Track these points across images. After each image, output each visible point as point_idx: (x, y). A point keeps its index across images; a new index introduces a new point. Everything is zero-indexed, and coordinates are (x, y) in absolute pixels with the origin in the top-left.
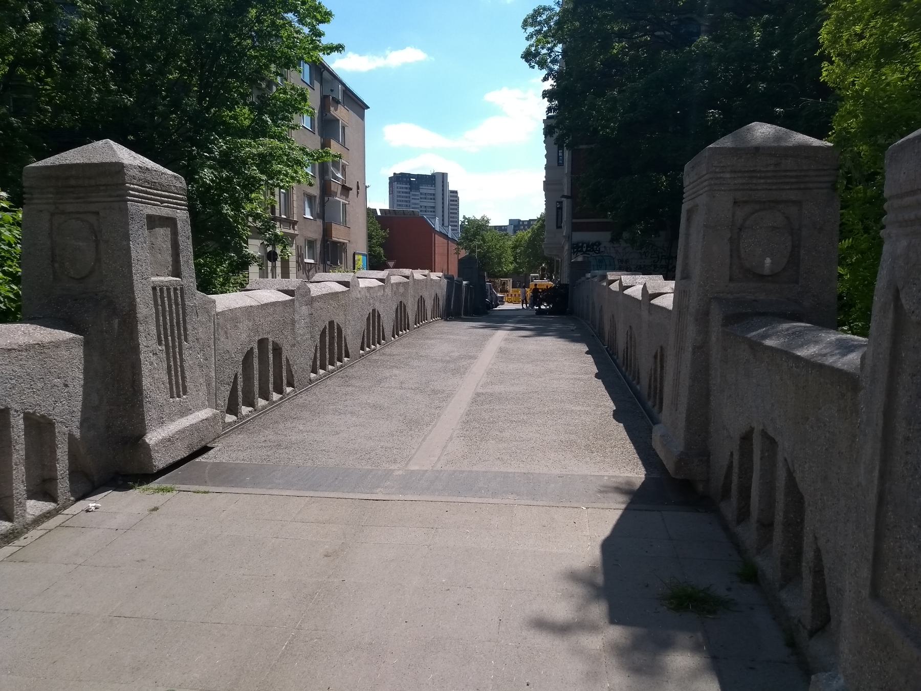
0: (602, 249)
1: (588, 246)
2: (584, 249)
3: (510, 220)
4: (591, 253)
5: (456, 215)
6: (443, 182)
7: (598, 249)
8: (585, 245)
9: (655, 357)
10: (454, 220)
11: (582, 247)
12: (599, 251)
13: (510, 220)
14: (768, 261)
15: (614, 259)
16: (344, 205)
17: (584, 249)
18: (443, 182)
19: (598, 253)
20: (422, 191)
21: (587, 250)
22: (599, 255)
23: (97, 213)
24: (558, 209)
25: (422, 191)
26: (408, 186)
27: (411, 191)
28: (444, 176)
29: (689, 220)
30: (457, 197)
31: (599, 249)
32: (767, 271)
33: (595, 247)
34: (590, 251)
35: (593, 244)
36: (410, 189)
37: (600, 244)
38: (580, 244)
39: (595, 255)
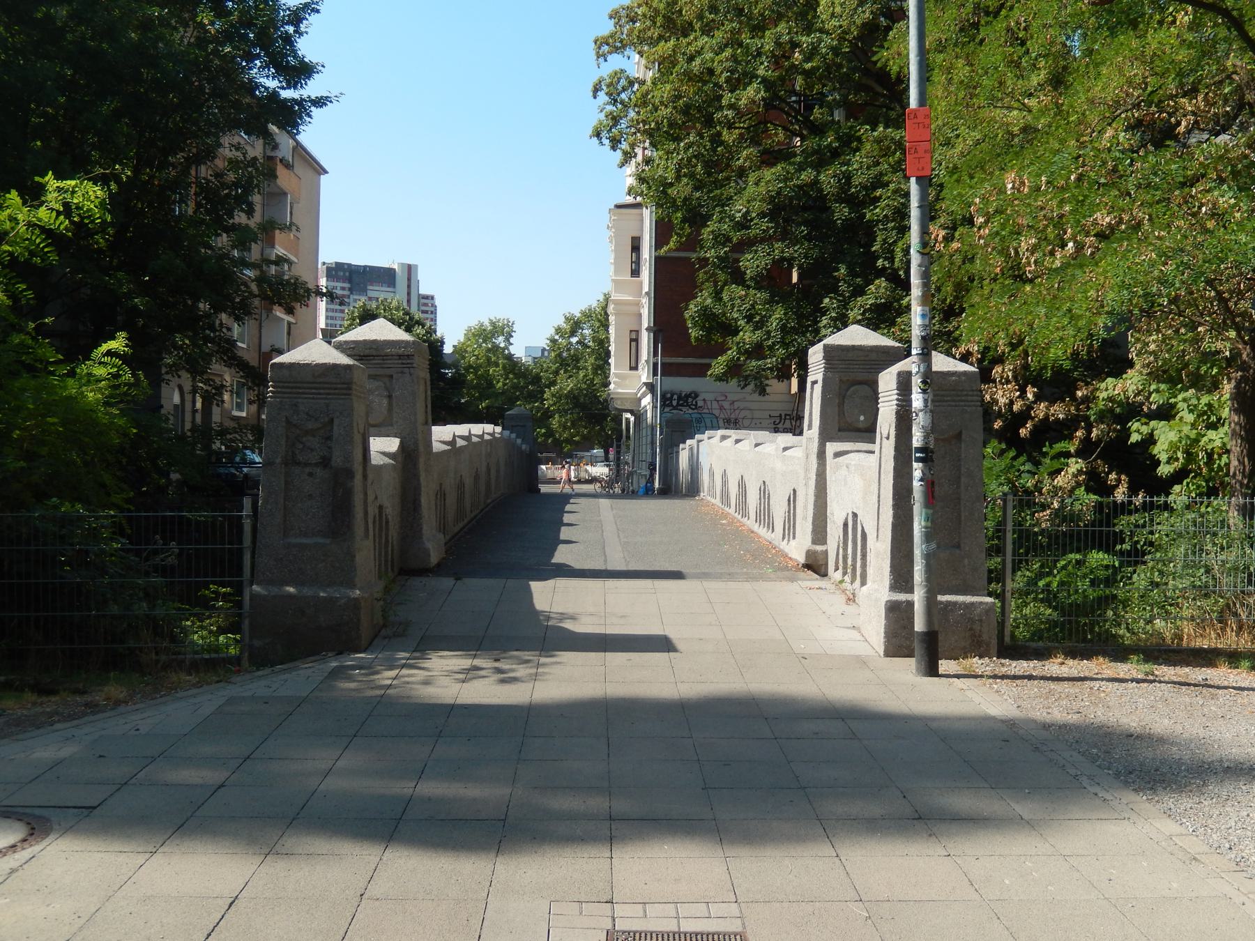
0: (700, 403)
1: (680, 398)
2: (675, 403)
3: (526, 347)
4: (684, 409)
5: (330, 314)
6: (409, 279)
7: (694, 403)
8: (675, 397)
9: (789, 500)
10: (332, 322)
11: (671, 399)
12: (696, 405)
13: (526, 347)
14: (862, 418)
15: (717, 418)
16: (289, 324)
17: (675, 403)
18: (409, 279)
19: (211, 380)
20: (371, 294)
21: (678, 404)
22: (696, 411)
23: (391, 376)
24: (631, 340)
25: (371, 294)
26: (347, 285)
27: (352, 293)
28: (410, 270)
29: (812, 388)
30: (434, 306)
31: (696, 402)
32: (861, 426)
33: (690, 400)
34: (682, 405)
35: (688, 396)
36: (350, 290)
37: (697, 396)
38: (669, 396)
39: (690, 411)
